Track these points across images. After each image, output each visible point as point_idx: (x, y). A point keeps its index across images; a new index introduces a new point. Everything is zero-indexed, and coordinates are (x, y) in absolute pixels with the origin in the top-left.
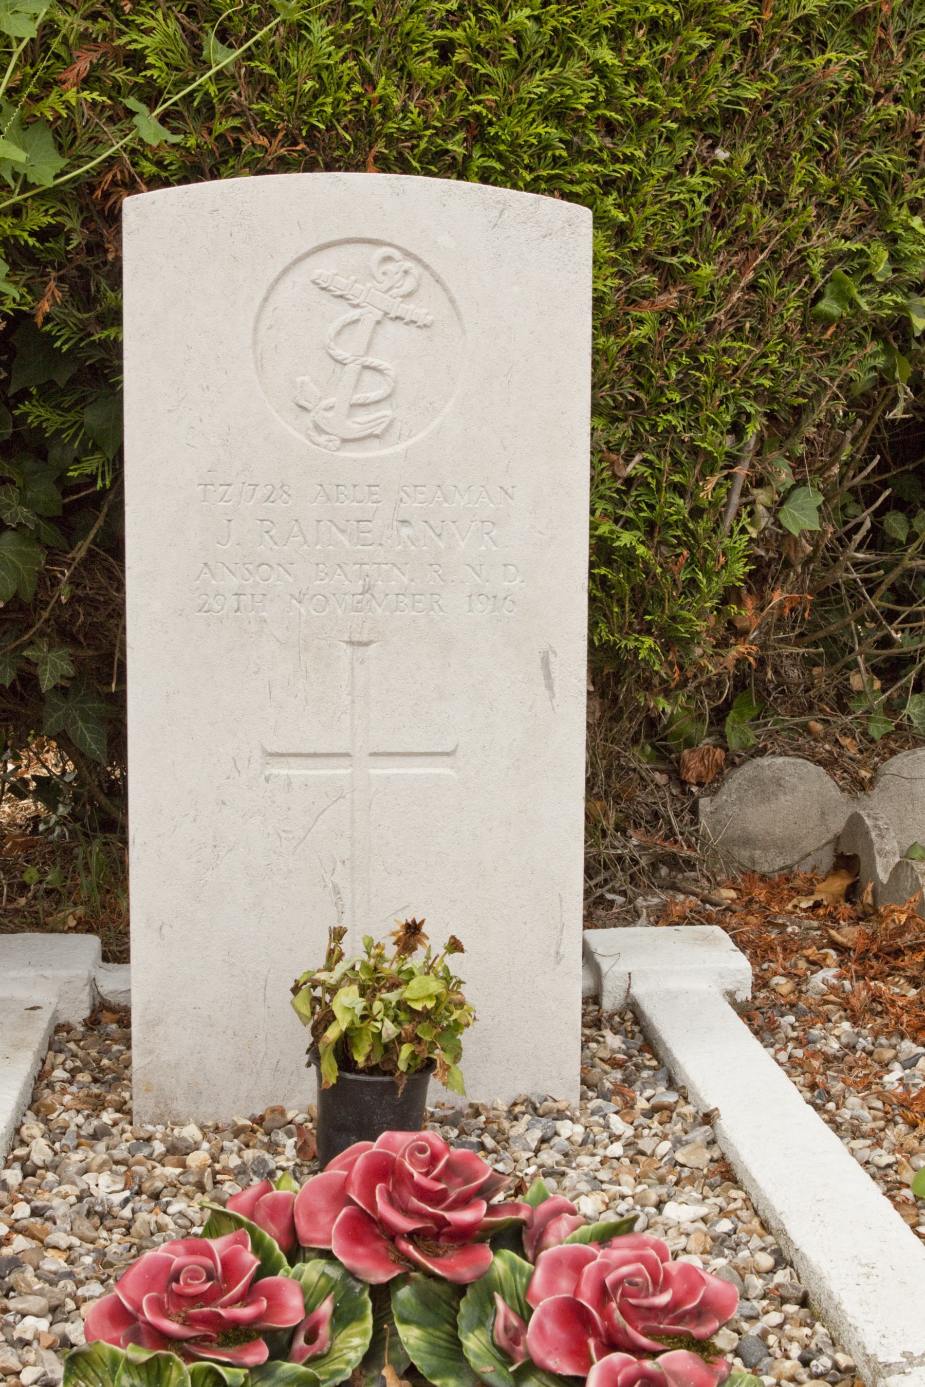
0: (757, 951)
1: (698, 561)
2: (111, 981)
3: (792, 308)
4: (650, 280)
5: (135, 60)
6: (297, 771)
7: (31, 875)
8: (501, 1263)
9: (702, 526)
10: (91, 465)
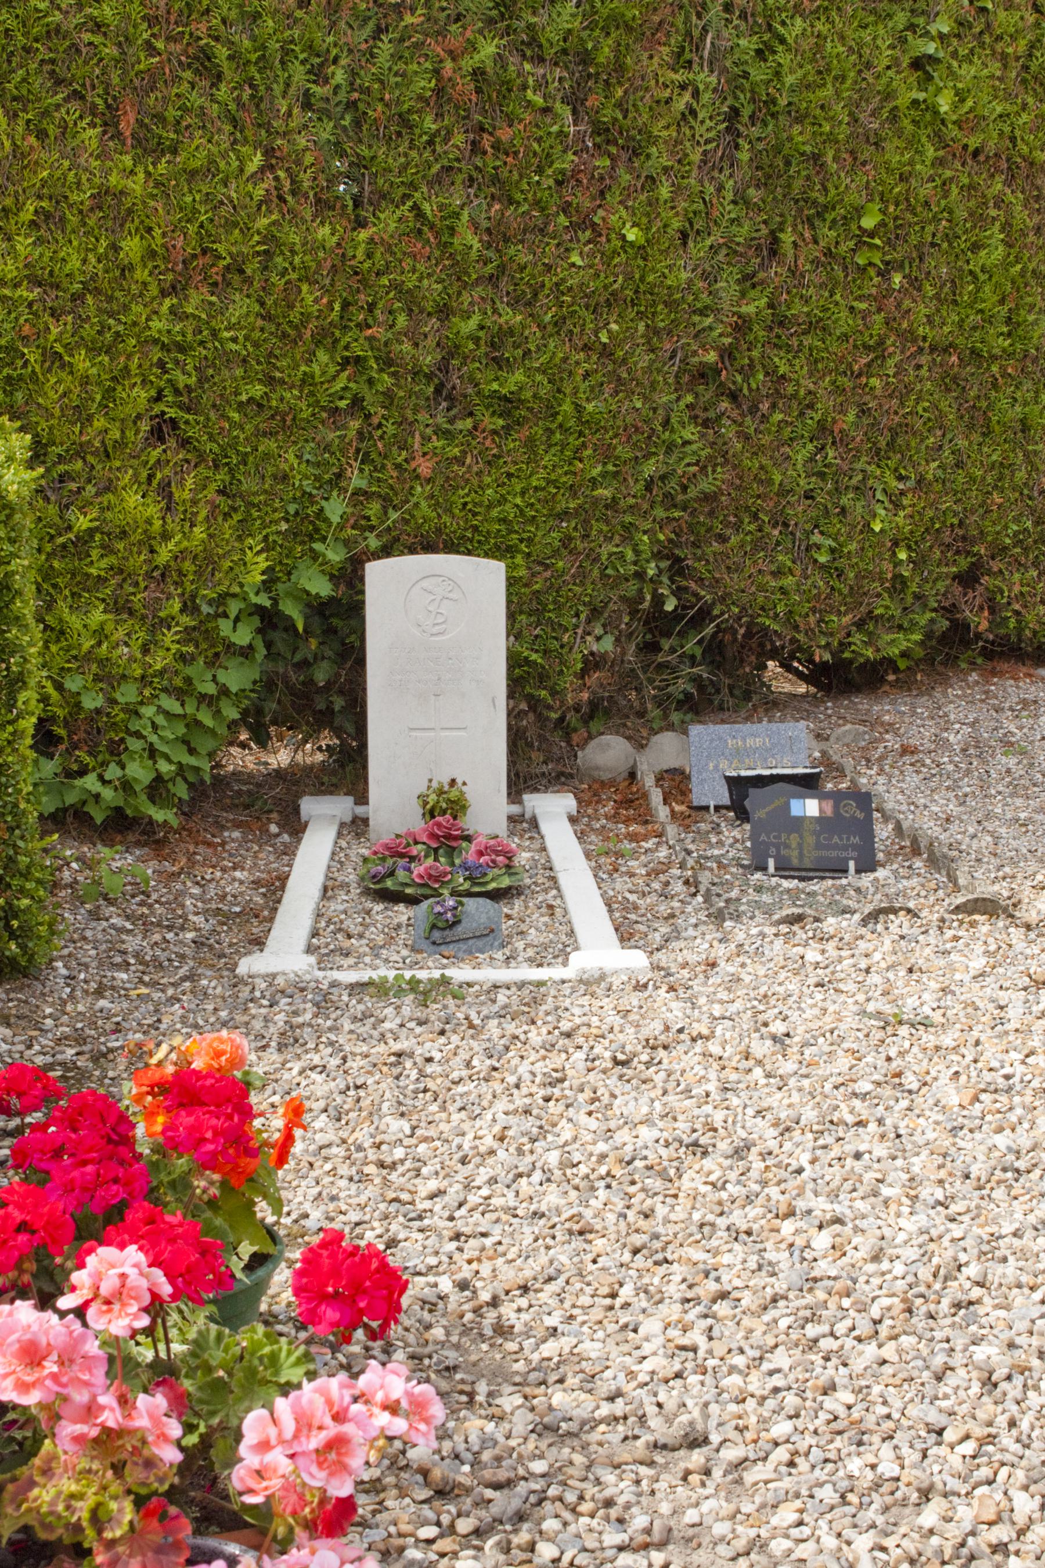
0: (579, 801)
1: (563, 663)
2: (360, 810)
3: (596, 573)
4: (539, 568)
5: (368, 519)
6: (418, 734)
7: (326, 779)
8: (464, 844)
9: (564, 651)
10: (353, 638)
